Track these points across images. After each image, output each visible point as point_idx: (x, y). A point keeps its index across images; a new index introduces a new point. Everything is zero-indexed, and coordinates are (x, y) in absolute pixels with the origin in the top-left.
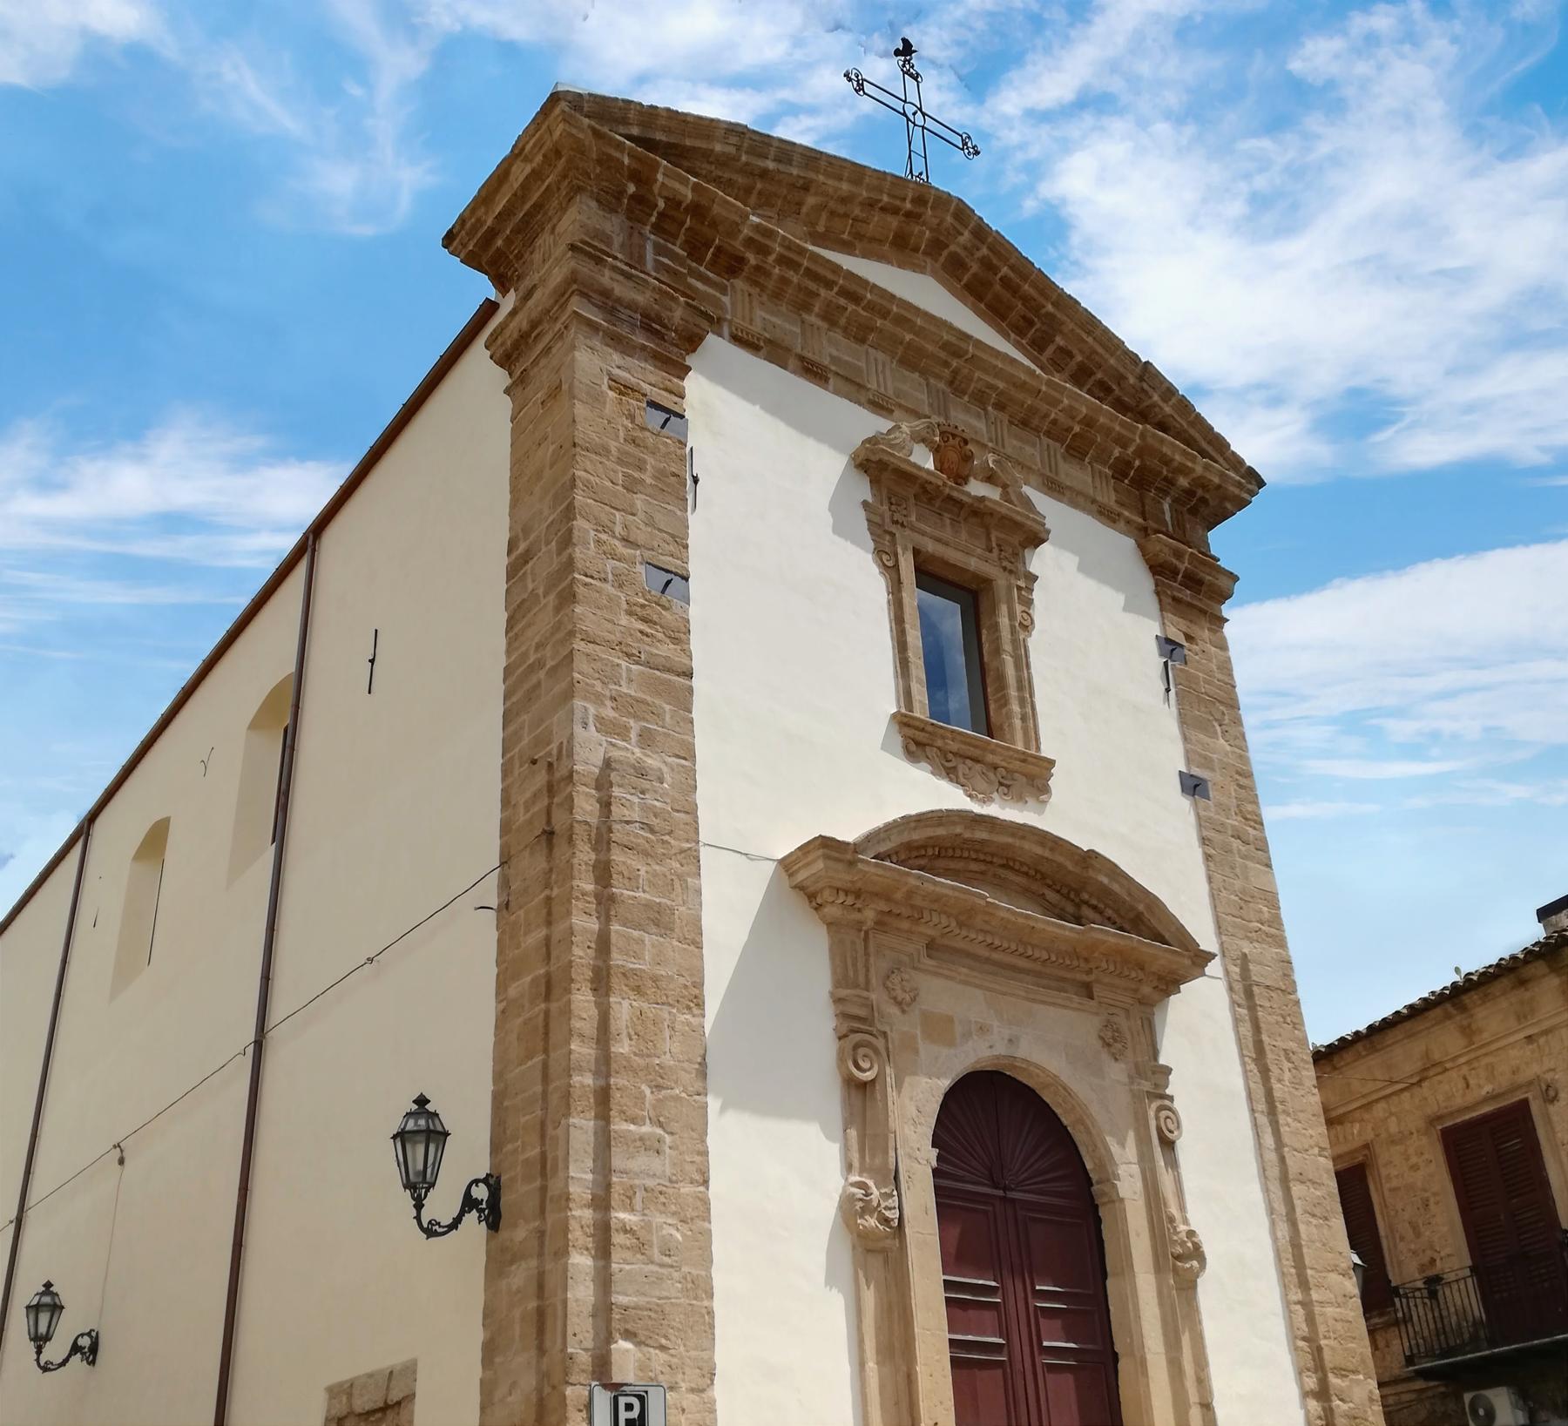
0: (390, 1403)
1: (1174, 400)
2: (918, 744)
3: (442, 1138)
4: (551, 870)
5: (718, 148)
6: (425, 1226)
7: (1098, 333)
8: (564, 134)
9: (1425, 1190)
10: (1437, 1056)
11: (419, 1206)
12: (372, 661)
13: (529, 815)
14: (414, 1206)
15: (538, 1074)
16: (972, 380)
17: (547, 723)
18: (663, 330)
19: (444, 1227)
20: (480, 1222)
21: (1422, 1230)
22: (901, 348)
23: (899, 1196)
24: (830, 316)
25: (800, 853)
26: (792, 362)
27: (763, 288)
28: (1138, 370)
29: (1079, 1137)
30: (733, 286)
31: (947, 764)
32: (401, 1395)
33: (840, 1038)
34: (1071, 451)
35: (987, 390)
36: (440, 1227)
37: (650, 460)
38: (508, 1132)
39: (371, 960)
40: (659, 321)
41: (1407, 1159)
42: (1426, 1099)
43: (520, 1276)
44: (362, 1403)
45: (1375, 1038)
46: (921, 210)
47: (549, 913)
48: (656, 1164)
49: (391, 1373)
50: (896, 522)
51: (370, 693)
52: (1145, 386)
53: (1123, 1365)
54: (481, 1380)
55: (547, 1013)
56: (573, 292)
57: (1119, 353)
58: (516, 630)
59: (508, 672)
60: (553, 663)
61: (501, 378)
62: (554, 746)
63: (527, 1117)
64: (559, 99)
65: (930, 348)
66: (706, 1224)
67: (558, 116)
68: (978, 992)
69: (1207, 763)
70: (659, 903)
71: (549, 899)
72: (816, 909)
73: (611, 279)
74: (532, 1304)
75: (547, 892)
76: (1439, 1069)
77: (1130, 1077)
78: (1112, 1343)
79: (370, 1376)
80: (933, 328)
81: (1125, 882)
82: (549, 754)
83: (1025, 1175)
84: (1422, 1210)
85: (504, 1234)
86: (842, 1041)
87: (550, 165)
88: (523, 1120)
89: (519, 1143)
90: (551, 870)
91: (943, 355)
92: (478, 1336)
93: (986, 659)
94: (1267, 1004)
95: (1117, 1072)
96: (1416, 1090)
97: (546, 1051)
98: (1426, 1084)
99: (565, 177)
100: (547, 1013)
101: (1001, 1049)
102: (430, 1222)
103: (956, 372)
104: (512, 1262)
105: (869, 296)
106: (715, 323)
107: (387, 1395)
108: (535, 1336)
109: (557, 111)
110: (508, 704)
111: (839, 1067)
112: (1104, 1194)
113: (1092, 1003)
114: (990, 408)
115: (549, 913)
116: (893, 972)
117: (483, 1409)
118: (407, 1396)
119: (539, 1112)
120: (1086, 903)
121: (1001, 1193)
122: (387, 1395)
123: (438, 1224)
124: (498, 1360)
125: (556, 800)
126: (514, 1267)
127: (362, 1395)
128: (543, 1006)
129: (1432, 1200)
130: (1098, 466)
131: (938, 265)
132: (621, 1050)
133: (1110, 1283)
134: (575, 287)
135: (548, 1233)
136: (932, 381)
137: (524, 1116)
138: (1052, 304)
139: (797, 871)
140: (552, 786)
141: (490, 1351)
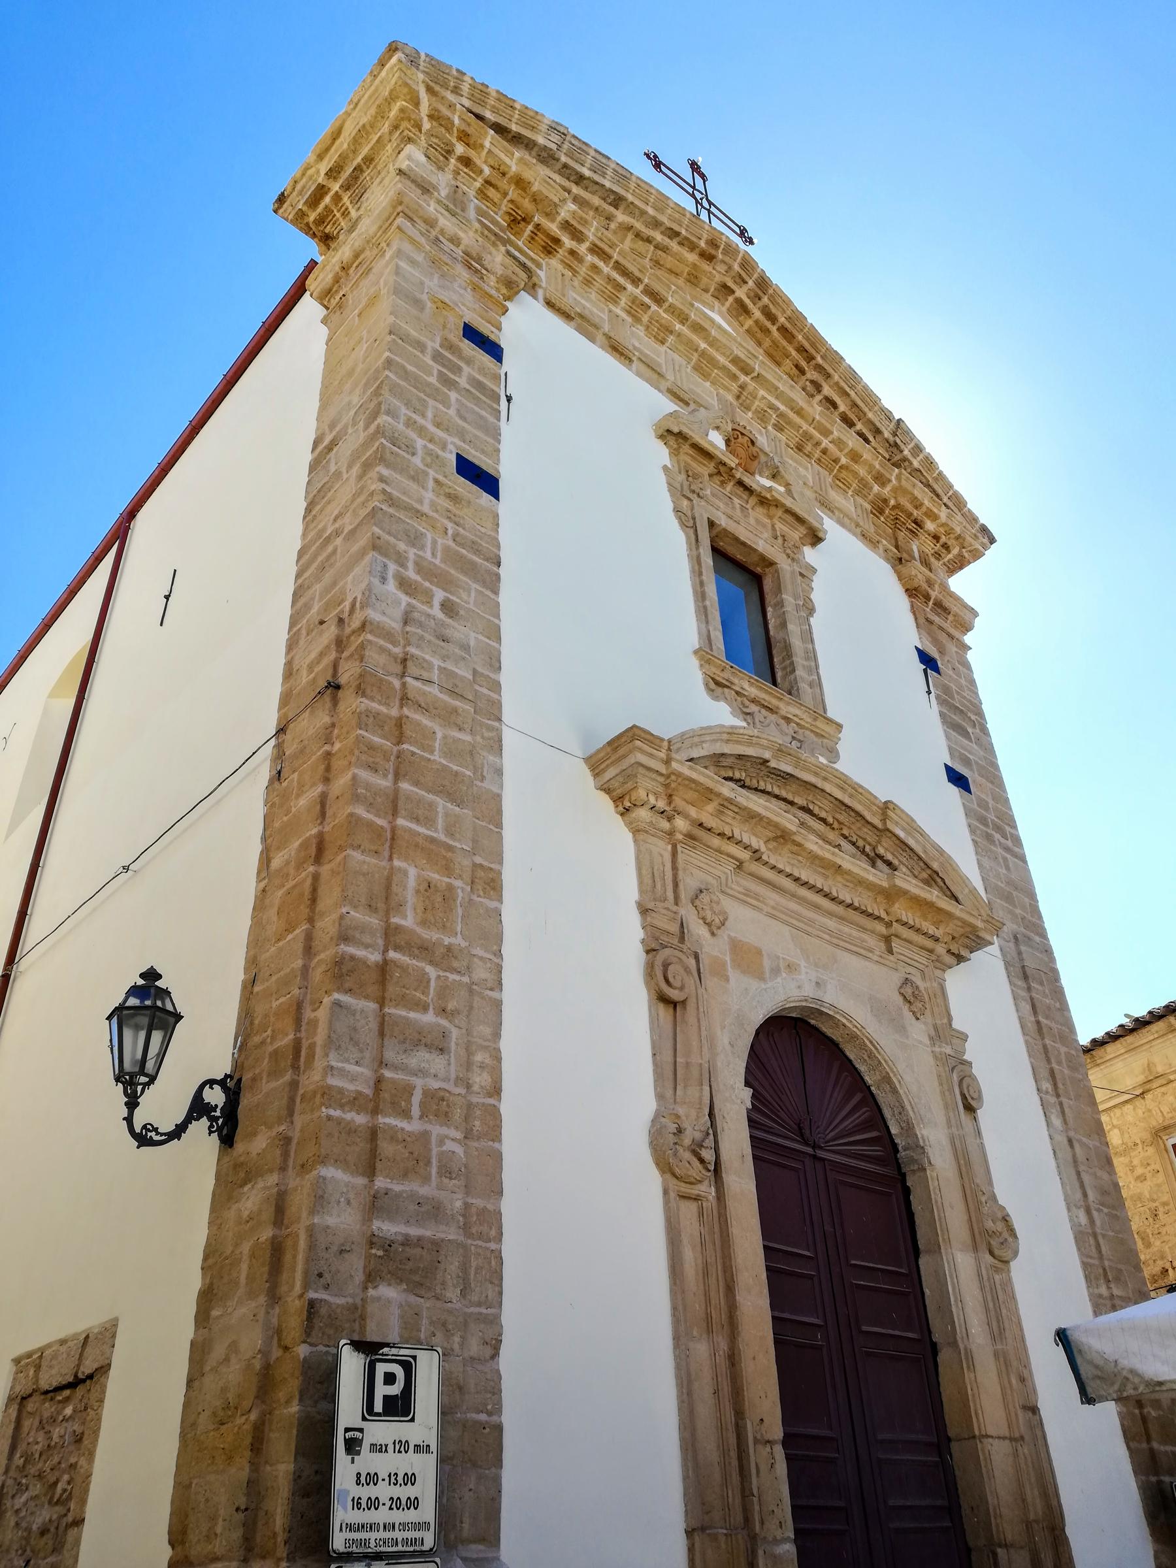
0: (80, 1376)
1: (921, 456)
2: (717, 683)
3: (172, 1020)
4: (333, 725)
5: (541, 140)
6: (138, 1130)
7: (859, 387)
8: (400, 83)
9: (1154, 1200)
10: (1160, 1069)
11: (132, 1104)
12: (167, 597)
13: (312, 675)
14: (126, 1104)
15: (299, 947)
16: (755, 398)
17: (341, 584)
18: (484, 272)
19: (162, 1134)
20: (210, 1133)
21: (1152, 1240)
22: (696, 355)
23: (715, 1135)
24: (636, 309)
25: (609, 749)
26: (600, 337)
27: (575, 272)
28: (892, 426)
29: (884, 1098)
30: (548, 264)
31: (745, 710)
32: (96, 1366)
33: (648, 952)
34: (838, 482)
35: (768, 410)
36: (158, 1133)
37: (466, 370)
38: (256, 1022)
39: (126, 868)
40: (479, 260)
41: (1132, 1171)
42: (1150, 1111)
43: (252, 1199)
44: (49, 1379)
45: (1098, 1052)
46: (713, 252)
47: (328, 769)
48: (437, 1063)
49: (87, 1337)
50: (693, 492)
51: (161, 625)
52: (898, 441)
53: (944, 1356)
54: (192, 1343)
55: (316, 877)
56: (398, 214)
57: (876, 408)
58: (314, 513)
59: (301, 554)
60: (350, 527)
61: (321, 312)
62: (347, 605)
63: (282, 1000)
64: (396, 49)
65: (722, 360)
66: (496, 1145)
67: (395, 65)
68: (786, 930)
69: (967, 762)
70: (457, 774)
71: (328, 754)
72: (622, 814)
73: (436, 210)
74: (267, 1234)
75: (327, 747)
76: (1162, 1081)
77: (931, 1038)
78: (930, 1332)
79: (63, 1342)
80: (724, 341)
81: (921, 839)
82: (342, 611)
83: (832, 1134)
84: (1151, 1220)
85: (240, 1147)
86: (650, 955)
87: (383, 117)
88: (275, 1004)
89: (269, 1032)
90: (333, 725)
91: (733, 369)
92: (196, 1282)
93: (772, 633)
94: (1040, 988)
95: (919, 1031)
96: (1138, 1102)
97: (311, 920)
98: (1148, 1096)
99: (396, 127)
100: (316, 877)
101: (809, 991)
102: (144, 1127)
103: (742, 387)
104: (245, 1183)
105: (670, 299)
106: (532, 288)
107: (78, 1366)
108: (265, 1276)
109: (394, 60)
110: (300, 581)
111: (647, 984)
112: (913, 1161)
113: (891, 958)
114: (770, 428)
115: (328, 769)
116: (701, 891)
117: (190, 1382)
118: (102, 1367)
119: (296, 991)
120: (881, 857)
121: (809, 1150)
122: (78, 1366)
123: (156, 1130)
124: (215, 1313)
125: (344, 655)
126: (246, 1189)
127: (51, 1367)
128: (311, 869)
129: (1161, 1210)
130: (860, 500)
131: (724, 309)
132: (403, 922)
133: (923, 1261)
134: (400, 208)
135: (295, 1141)
136: (721, 391)
137: (277, 999)
138: (821, 356)
139: (604, 770)
140: (342, 641)
141: (207, 1299)
